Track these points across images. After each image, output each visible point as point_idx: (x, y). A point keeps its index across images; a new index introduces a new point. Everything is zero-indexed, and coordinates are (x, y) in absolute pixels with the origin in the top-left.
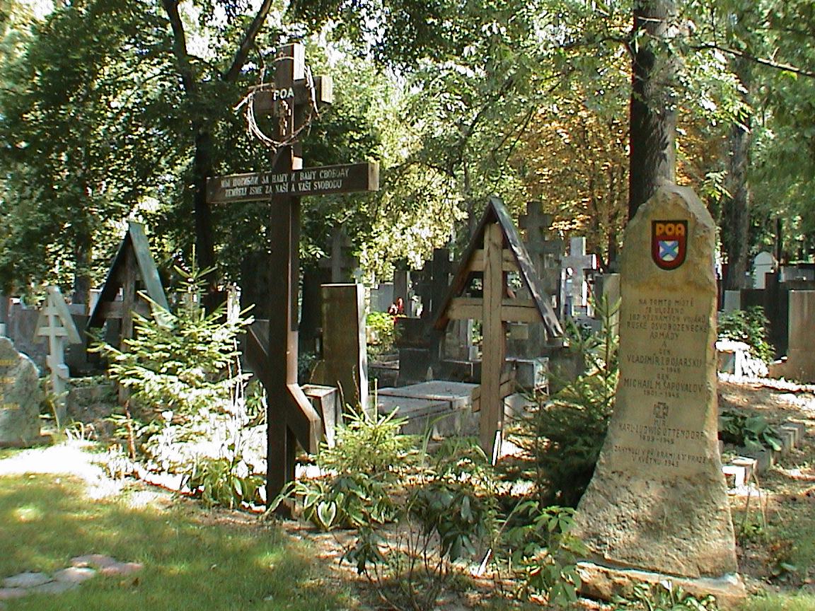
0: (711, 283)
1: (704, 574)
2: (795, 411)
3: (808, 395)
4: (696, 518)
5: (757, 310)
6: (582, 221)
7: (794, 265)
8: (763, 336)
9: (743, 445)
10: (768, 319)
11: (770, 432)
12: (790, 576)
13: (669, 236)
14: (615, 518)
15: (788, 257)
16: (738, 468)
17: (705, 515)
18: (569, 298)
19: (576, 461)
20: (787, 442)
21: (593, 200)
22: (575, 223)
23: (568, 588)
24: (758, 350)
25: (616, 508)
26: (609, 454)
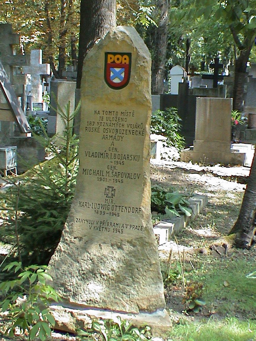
0: (147, 100)
1: (142, 310)
2: (199, 186)
3: (209, 175)
4: (136, 270)
5: (172, 110)
6: (39, 37)
7: (198, 74)
8: (177, 130)
9: (164, 213)
10: (180, 117)
11: (183, 203)
12: (201, 309)
13: (118, 64)
14: (77, 272)
15: (194, 69)
16: (161, 232)
17: (142, 268)
18: (29, 98)
19: (46, 229)
20: (195, 209)
21: (48, 20)
22: (33, 38)
23: (45, 325)
24: (172, 140)
25: (78, 264)
26: (72, 225)
